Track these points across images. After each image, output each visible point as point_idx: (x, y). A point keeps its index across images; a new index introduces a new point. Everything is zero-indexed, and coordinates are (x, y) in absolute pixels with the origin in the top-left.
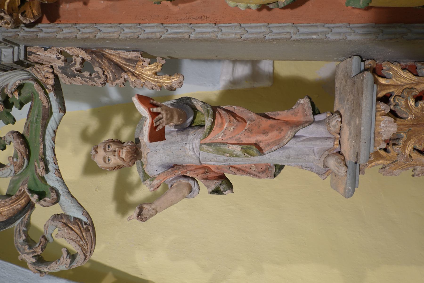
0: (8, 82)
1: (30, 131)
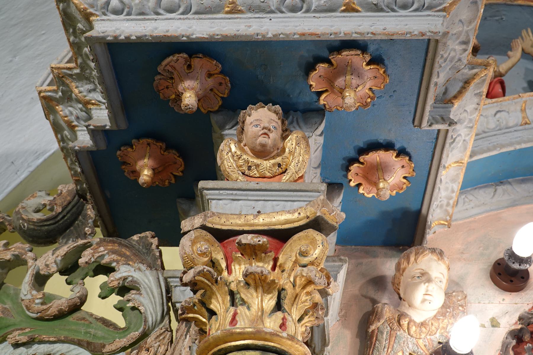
0: (145, 295)
1: (78, 321)
